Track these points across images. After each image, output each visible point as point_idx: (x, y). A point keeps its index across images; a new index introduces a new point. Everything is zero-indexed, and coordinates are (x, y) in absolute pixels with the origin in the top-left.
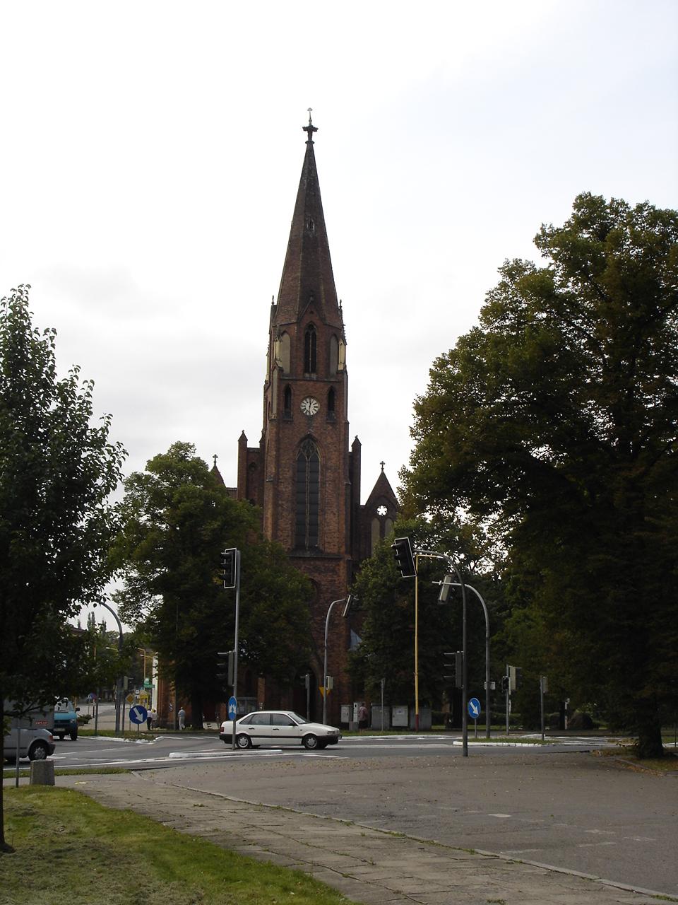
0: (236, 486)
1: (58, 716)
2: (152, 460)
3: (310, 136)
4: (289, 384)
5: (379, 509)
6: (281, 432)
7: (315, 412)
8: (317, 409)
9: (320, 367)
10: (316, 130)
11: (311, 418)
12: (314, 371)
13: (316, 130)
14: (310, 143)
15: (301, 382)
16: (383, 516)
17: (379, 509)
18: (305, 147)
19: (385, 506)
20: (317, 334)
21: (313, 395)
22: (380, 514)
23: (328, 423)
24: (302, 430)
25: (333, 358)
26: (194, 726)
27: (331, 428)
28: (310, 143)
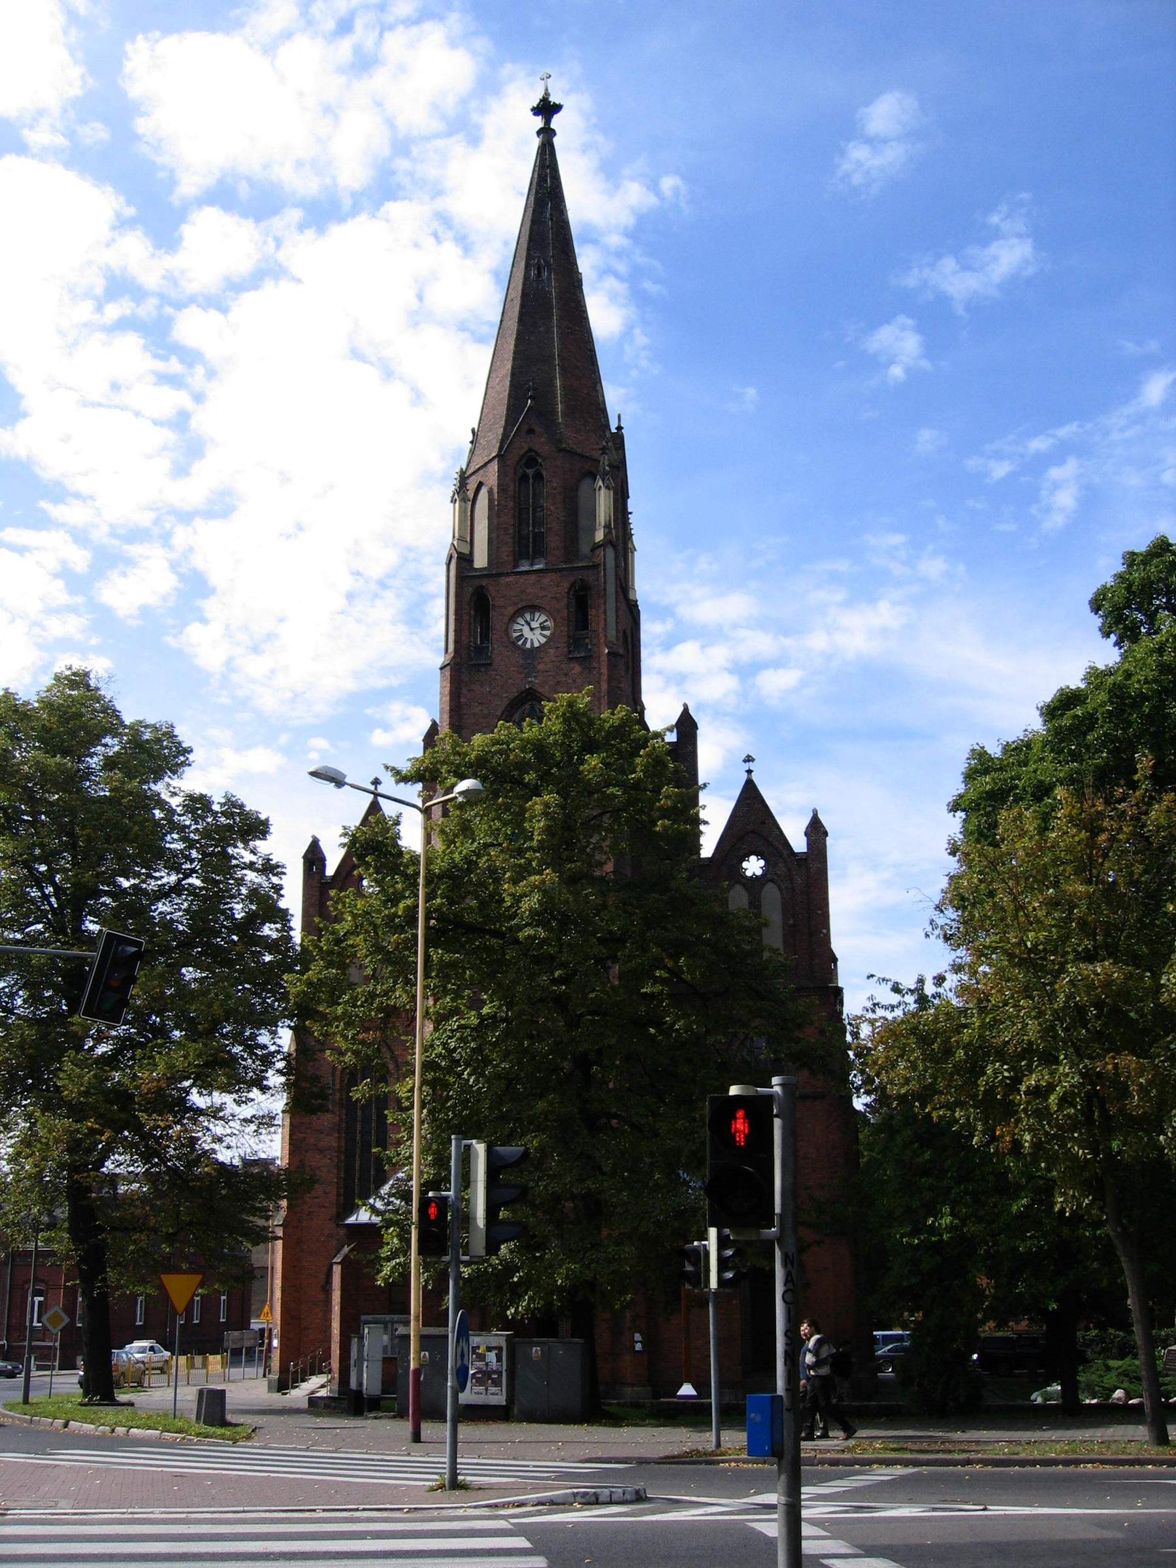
0: (805, 850)
1: (380, 1218)
2: (995, 750)
3: (548, 121)
4: (482, 587)
5: (745, 865)
6: (464, 691)
7: (543, 640)
8: (547, 633)
9: (554, 542)
10: (557, 108)
11: (533, 654)
12: (539, 553)
13: (557, 108)
14: (547, 133)
15: (511, 579)
16: (755, 878)
17: (745, 865)
18: (536, 142)
19: (760, 854)
20: (544, 473)
21: (537, 602)
22: (749, 874)
23: (571, 659)
24: (510, 681)
25: (583, 522)
26: (278, 1391)
27: (577, 669)
28: (547, 133)
